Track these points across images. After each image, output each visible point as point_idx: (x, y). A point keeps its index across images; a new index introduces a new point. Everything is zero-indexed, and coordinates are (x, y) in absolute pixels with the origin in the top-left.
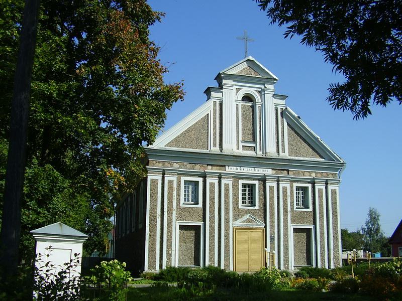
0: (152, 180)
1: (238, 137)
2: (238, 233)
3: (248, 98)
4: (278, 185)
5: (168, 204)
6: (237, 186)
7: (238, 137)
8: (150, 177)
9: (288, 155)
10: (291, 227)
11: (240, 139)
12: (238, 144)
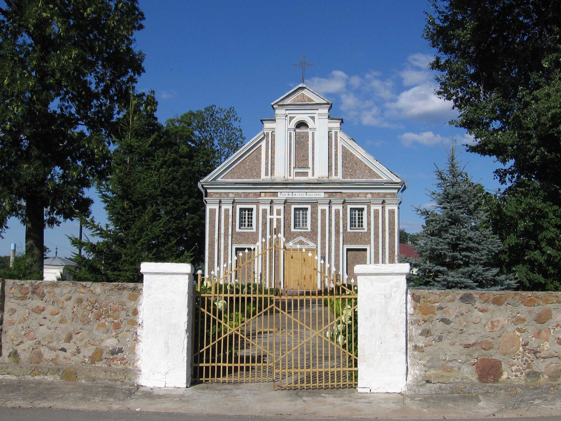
0: (389, 210)
1: (290, 164)
2: (350, 253)
3: (301, 124)
4: (220, 207)
5: (225, 229)
6: (346, 209)
7: (290, 164)
8: (208, 207)
9: (341, 178)
10: (343, 249)
11: (293, 165)
12: (290, 171)
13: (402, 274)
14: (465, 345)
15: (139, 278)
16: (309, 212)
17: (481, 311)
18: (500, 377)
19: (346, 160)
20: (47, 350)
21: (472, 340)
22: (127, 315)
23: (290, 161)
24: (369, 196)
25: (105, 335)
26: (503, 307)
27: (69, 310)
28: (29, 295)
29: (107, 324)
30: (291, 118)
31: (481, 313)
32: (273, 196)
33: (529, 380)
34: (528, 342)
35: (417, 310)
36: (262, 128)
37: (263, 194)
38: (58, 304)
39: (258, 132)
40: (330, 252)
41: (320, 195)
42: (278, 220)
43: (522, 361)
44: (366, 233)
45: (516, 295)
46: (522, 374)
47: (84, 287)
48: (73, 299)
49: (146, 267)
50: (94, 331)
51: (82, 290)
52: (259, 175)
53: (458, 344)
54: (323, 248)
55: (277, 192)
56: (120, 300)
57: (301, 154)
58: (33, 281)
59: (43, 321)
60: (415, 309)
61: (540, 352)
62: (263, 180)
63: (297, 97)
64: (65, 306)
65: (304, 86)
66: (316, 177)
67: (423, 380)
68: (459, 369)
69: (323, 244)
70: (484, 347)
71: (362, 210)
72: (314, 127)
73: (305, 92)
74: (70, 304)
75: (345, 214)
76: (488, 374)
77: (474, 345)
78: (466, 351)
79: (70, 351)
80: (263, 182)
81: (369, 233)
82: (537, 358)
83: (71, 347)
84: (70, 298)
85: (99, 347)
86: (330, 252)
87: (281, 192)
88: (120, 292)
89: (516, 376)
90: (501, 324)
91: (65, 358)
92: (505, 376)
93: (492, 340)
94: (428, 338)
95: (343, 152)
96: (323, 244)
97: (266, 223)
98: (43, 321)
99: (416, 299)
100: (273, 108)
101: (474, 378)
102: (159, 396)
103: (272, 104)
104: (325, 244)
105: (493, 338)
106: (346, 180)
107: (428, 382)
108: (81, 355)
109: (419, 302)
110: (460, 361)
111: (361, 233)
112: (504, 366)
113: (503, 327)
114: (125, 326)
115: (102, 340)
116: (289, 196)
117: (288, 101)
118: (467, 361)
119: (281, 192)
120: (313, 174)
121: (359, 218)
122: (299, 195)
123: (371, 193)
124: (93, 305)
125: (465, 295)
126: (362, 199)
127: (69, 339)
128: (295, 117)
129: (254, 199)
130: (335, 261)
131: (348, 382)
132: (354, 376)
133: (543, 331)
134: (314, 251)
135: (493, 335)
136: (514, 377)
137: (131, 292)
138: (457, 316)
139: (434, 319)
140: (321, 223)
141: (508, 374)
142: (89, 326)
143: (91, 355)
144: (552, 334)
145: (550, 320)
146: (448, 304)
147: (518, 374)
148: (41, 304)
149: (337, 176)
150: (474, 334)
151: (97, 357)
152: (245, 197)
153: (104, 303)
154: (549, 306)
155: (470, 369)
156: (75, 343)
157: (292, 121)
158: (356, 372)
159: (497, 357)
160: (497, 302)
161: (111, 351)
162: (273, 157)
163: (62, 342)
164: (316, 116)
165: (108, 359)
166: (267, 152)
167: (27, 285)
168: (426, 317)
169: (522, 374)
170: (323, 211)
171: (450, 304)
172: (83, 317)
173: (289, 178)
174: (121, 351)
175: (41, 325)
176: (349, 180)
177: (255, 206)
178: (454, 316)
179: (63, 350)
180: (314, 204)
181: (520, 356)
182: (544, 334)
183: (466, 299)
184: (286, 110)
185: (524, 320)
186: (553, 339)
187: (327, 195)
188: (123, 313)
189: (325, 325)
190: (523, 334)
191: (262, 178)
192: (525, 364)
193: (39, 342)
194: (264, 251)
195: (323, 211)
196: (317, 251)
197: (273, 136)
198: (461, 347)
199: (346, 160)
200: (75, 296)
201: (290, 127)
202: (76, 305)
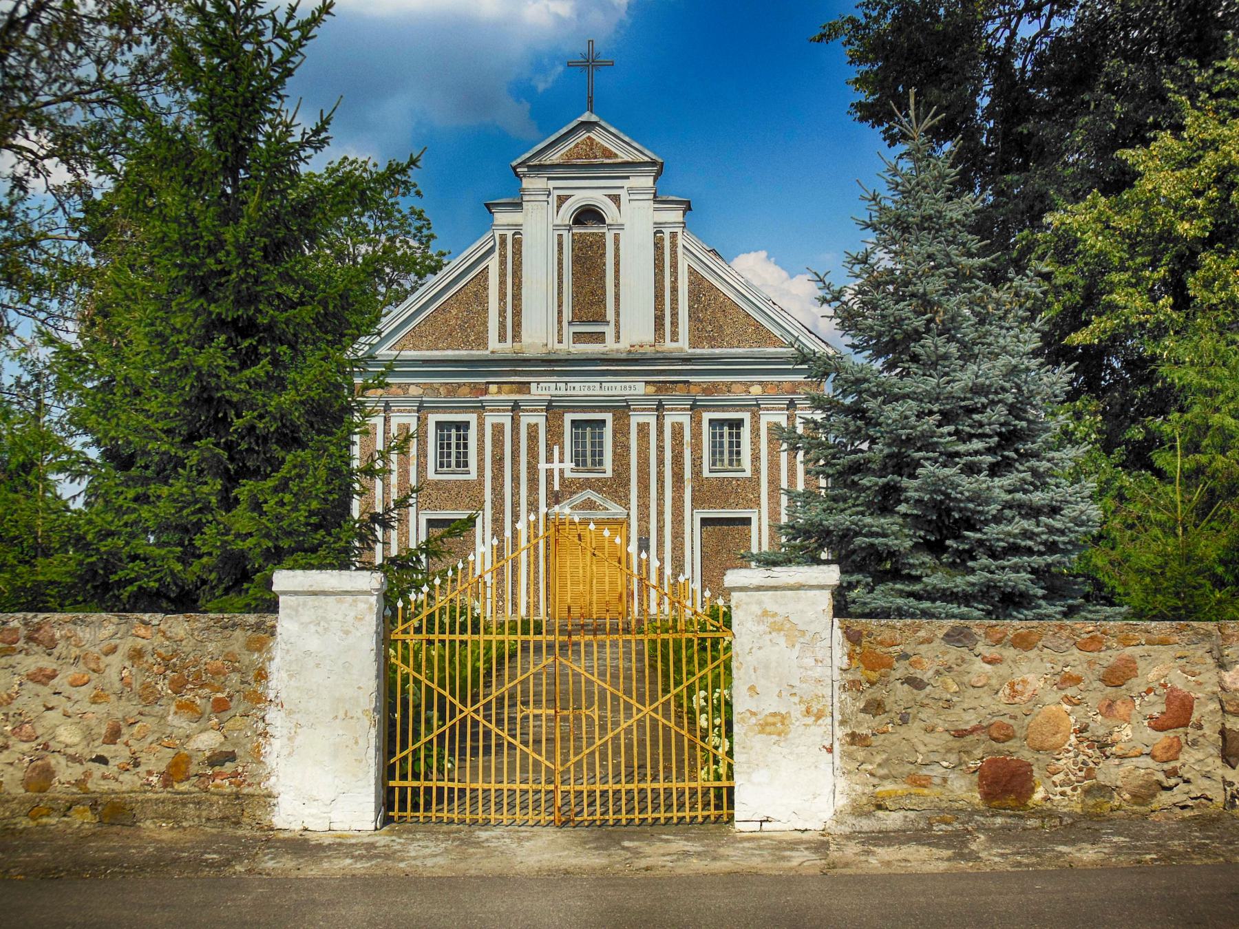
1: (560, 312)
3: (589, 215)
6: (699, 423)
7: (560, 312)
10: (692, 519)
11: (567, 314)
13: (822, 587)
14: (956, 731)
15: (272, 606)
16: (608, 431)
17: (989, 663)
18: (1030, 798)
19: (699, 302)
20: (63, 761)
21: (970, 720)
22: (242, 683)
23: (560, 306)
24: (756, 390)
25: (195, 725)
26: (1032, 654)
27: (112, 675)
28: (21, 644)
29: (198, 701)
30: (562, 200)
31: (988, 667)
32: (520, 392)
33: (1091, 802)
34: (1087, 726)
35: (856, 662)
36: (490, 225)
37: (493, 388)
38: (86, 664)
39: (482, 234)
40: (660, 529)
41: (637, 388)
42: (549, 460)
43: (1075, 764)
44: (750, 480)
45: (1061, 627)
46: (1074, 789)
47: (146, 624)
48: (120, 652)
49: (283, 580)
50: (170, 718)
51: (142, 632)
52: (482, 341)
53: (940, 729)
54: (644, 517)
55: (529, 383)
56: (226, 650)
57: (588, 289)
58: (30, 615)
59: (54, 701)
60: (850, 657)
61: (1112, 745)
62: (492, 352)
63: (576, 146)
64: (102, 666)
65: (594, 118)
66: (624, 345)
67: (869, 803)
68: (945, 780)
69: (644, 507)
70: (995, 735)
71: (738, 424)
72: (620, 222)
73: (597, 136)
74: (116, 660)
75: (696, 435)
76: (1006, 792)
77: (972, 731)
78: (956, 744)
79: (117, 762)
80: (496, 357)
81: (755, 481)
82: (1108, 757)
83: (118, 753)
84: (113, 650)
85: (182, 751)
86: (660, 529)
87: (538, 383)
88: (227, 632)
89: (1063, 794)
90: (1030, 688)
91: (104, 777)
92: (1039, 795)
93: (1012, 722)
94: (878, 718)
95: (691, 283)
96: (644, 507)
97: (502, 459)
98: (54, 701)
99: (852, 637)
100: (517, 174)
101: (977, 797)
102: (320, 847)
103: (514, 163)
104: (648, 507)
105: (1015, 718)
106: (698, 351)
107: (879, 807)
108: (142, 769)
109: (860, 645)
110: (945, 764)
111: (737, 479)
112: (1037, 775)
113: (1034, 695)
114: (238, 707)
115: (187, 736)
116: (558, 393)
117: (555, 157)
118: (960, 764)
119: (538, 383)
120: (618, 338)
121: (731, 443)
122: (582, 388)
123: (760, 383)
124: (166, 662)
125: (954, 628)
126: (738, 394)
127: (114, 735)
128: (570, 196)
129: (465, 396)
130: (673, 549)
131: (712, 812)
132: (725, 798)
133: (1119, 702)
134: (619, 524)
135: (1011, 710)
136: (1058, 797)
137: (249, 632)
138: (938, 673)
139: (892, 679)
140: (639, 457)
141: (1047, 791)
142: (157, 708)
143: (163, 768)
144: (1138, 708)
145: (1133, 680)
146: (920, 647)
147: (1068, 790)
148: (48, 663)
149: (677, 341)
150: (974, 709)
151: (176, 771)
152: (449, 394)
153: (191, 656)
154: (1129, 651)
155: (967, 781)
156: (126, 744)
157: (565, 206)
158: (731, 791)
159: (1027, 755)
160: (1023, 642)
161: (209, 758)
162: (517, 297)
163: (97, 743)
164: (623, 193)
165: (200, 776)
166: (502, 283)
167: (14, 624)
168: (874, 676)
169: (1074, 789)
170: (643, 429)
171: (923, 649)
172: (145, 689)
173: (557, 346)
174: (231, 757)
175: (48, 709)
176: (706, 351)
177: (475, 415)
178: (930, 673)
179: (102, 760)
180: (622, 410)
181: (1071, 754)
182: (1121, 709)
183: (957, 637)
184: (549, 179)
185: (1078, 680)
186: (1140, 719)
187: (651, 389)
188: (235, 678)
189: (576, 754)
190: (1077, 708)
191: (490, 349)
192: (1081, 770)
193: (46, 747)
194: (533, 542)
195: (643, 429)
196: (629, 525)
197: (517, 243)
198: (947, 737)
199: (699, 302)
200: (126, 645)
201: (558, 222)
202: (128, 664)
